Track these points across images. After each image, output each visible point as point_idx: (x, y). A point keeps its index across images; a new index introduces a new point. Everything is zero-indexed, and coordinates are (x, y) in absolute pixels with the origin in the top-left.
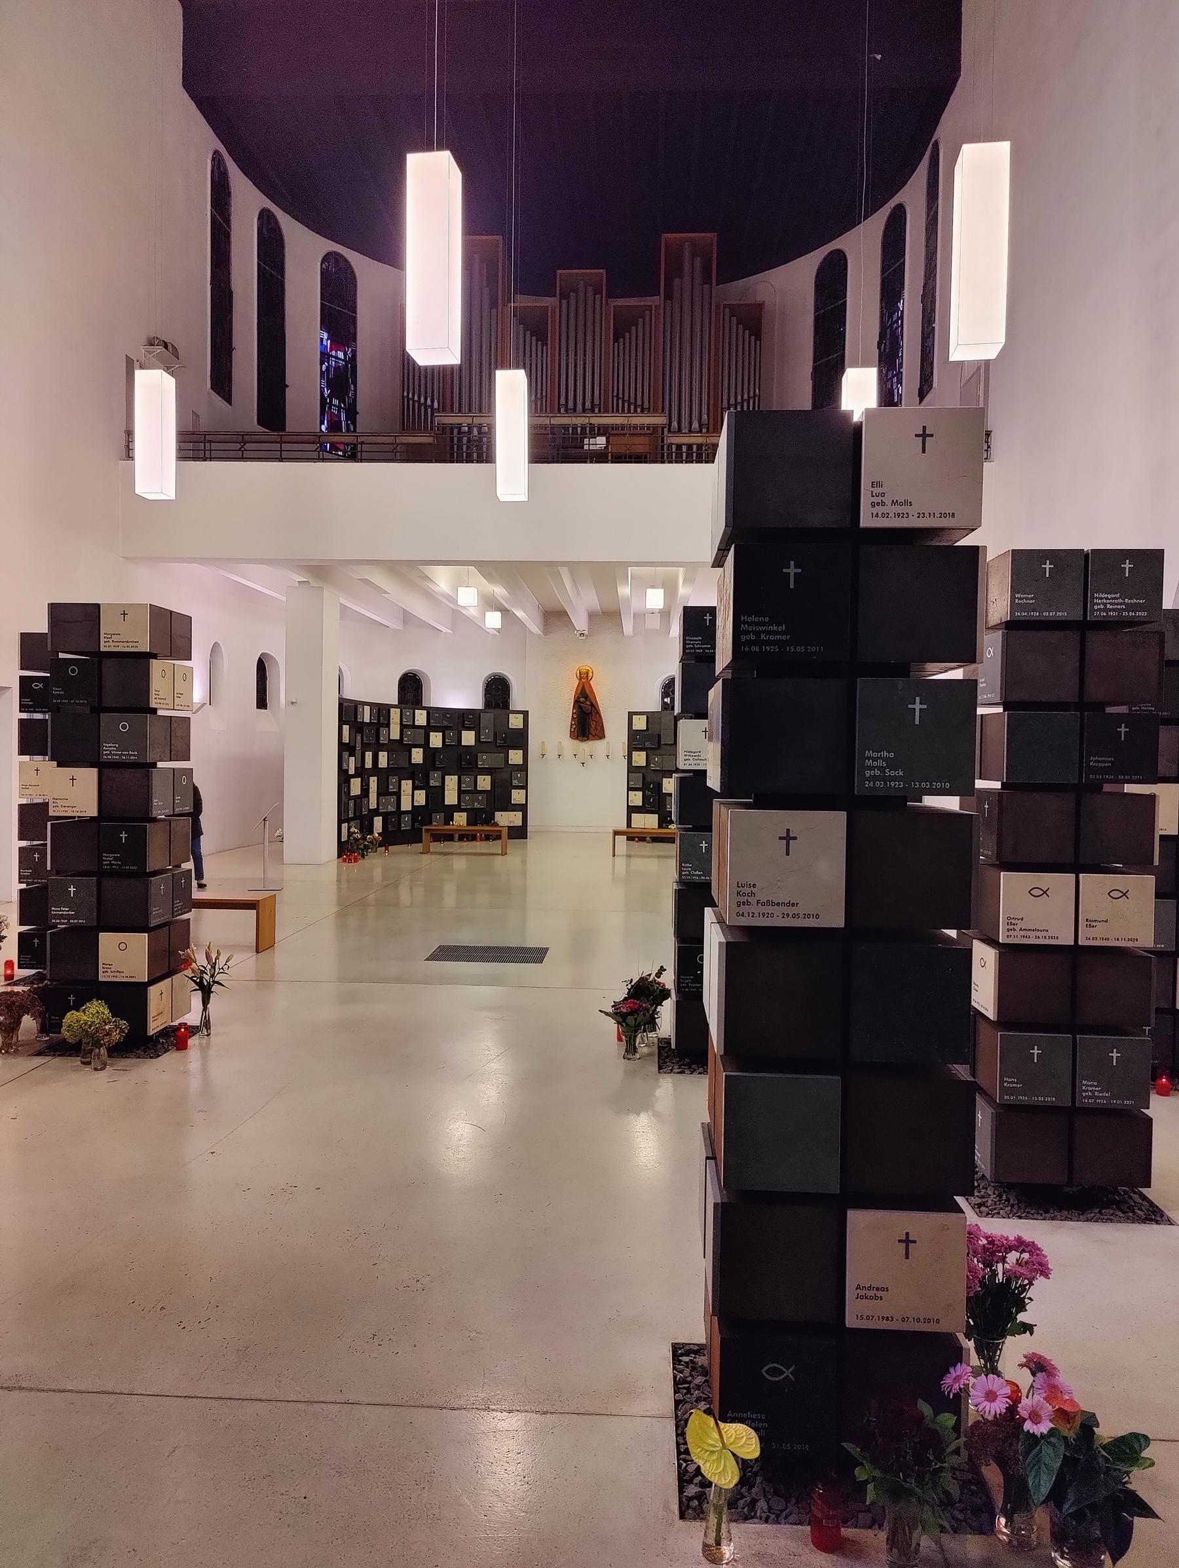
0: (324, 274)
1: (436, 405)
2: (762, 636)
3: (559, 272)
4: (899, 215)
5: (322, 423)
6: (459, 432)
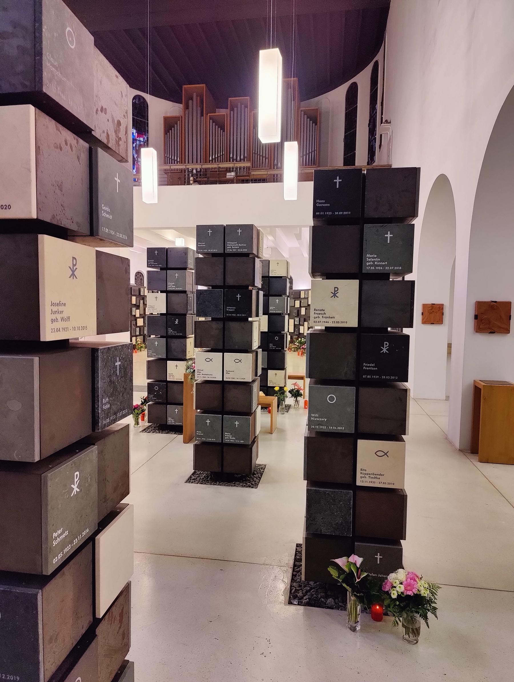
0: (134, 104)
1: (178, 160)
2: (376, 263)
3: (229, 99)
4: (376, 63)
5: (134, 169)
6: (188, 171)
